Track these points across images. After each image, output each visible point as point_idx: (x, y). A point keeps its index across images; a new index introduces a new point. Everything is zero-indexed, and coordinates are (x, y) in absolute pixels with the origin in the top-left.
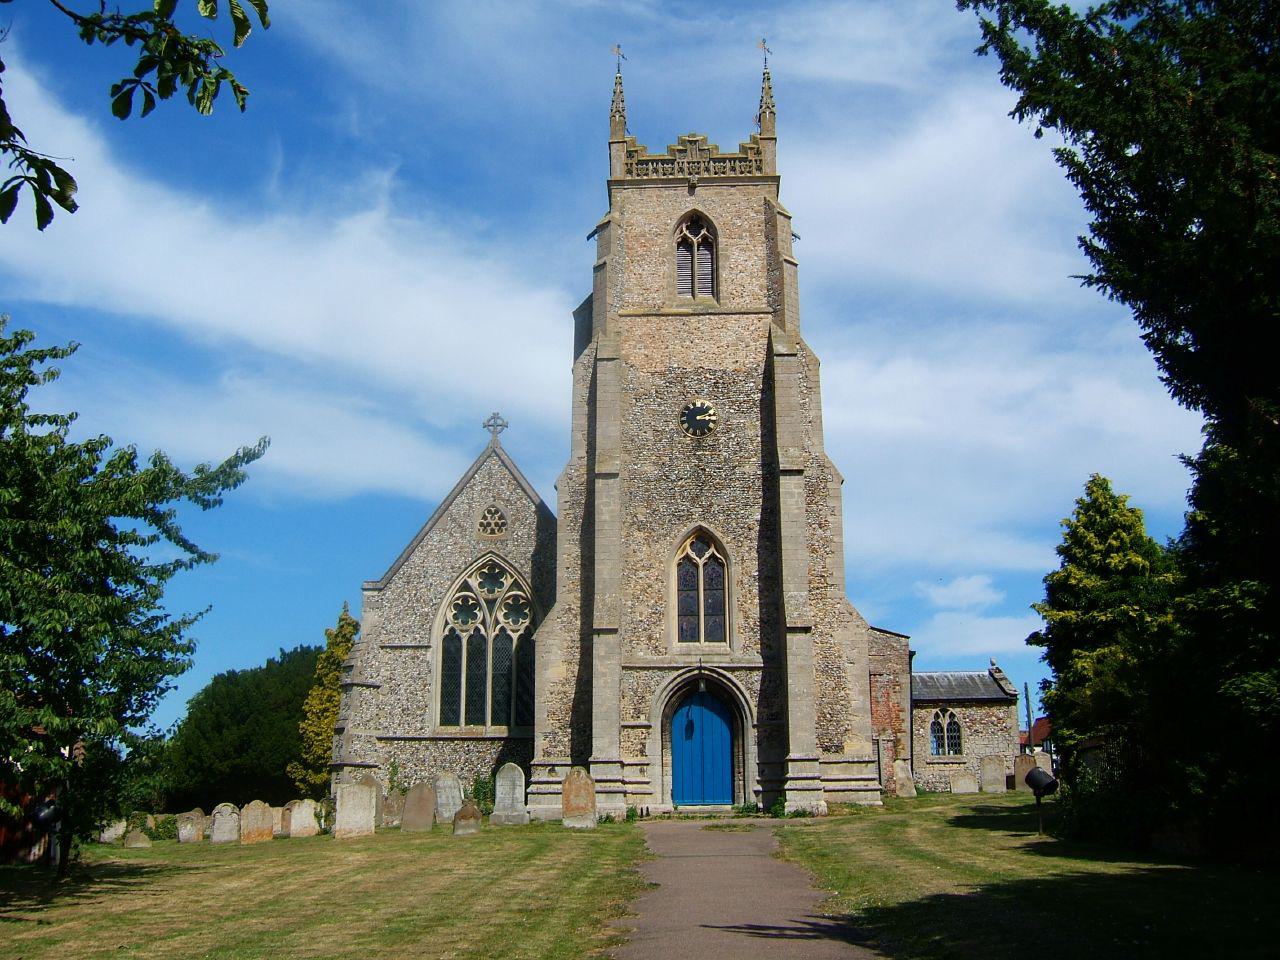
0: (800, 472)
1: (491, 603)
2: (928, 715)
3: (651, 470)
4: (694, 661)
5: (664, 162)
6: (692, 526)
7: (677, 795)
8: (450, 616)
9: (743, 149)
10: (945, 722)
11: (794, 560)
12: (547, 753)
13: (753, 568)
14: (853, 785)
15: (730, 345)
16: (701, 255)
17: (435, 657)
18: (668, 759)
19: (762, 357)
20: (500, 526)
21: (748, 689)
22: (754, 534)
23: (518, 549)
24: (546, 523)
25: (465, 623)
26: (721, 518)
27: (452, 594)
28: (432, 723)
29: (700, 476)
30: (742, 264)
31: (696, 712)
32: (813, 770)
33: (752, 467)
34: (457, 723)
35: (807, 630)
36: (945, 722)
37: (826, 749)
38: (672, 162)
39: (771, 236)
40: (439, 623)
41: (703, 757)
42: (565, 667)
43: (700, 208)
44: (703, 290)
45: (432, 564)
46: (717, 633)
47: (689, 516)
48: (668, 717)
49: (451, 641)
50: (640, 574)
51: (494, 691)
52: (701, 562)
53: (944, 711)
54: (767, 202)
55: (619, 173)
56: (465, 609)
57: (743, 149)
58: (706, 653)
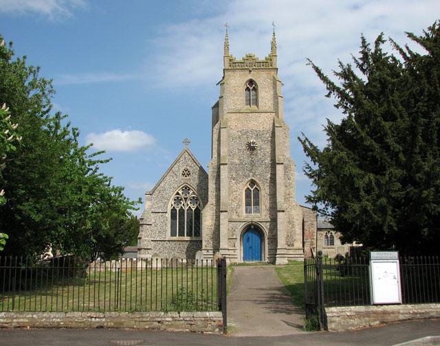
0: (282, 164)
1: (186, 199)
2: (324, 233)
3: (237, 161)
4: (249, 219)
5: (241, 63)
6: (250, 179)
7: (244, 259)
8: (173, 203)
9: (266, 59)
10: (329, 235)
11: (280, 190)
12: (206, 246)
13: (268, 191)
14: (296, 256)
15: (262, 122)
16: (252, 93)
17: (169, 215)
18: (242, 248)
19: (271, 126)
20: (188, 175)
21: (266, 228)
22: (268, 181)
23: (194, 181)
24: (203, 175)
25: (178, 205)
26: (258, 176)
27: (174, 196)
28: (168, 236)
29: (252, 164)
30: (265, 96)
31: (250, 234)
32: (285, 252)
33: (268, 161)
34: (175, 235)
35: (283, 211)
36: (329, 235)
37: (289, 246)
38: (244, 63)
39: (275, 87)
40: (170, 204)
41: (219, 140)
42: (211, 221)
43: (254, 79)
44: (253, 103)
45: (167, 186)
46: (257, 211)
47: (249, 176)
48: (242, 235)
49: (173, 210)
50: (233, 191)
51: (188, 224)
52: (252, 190)
53: (329, 232)
54: (274, 77)
55: (227, 67)
56: (178, 200)
57: (266, 59)
58: (254, 217)
